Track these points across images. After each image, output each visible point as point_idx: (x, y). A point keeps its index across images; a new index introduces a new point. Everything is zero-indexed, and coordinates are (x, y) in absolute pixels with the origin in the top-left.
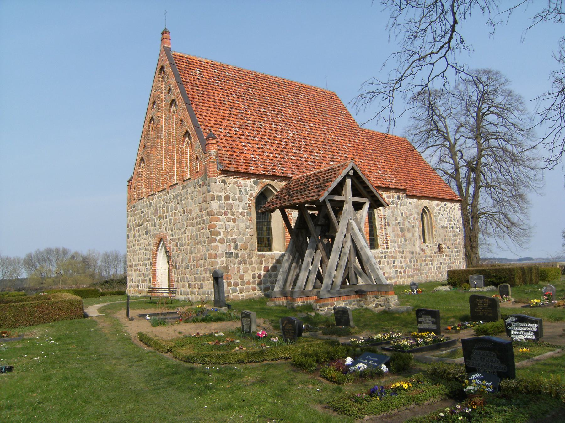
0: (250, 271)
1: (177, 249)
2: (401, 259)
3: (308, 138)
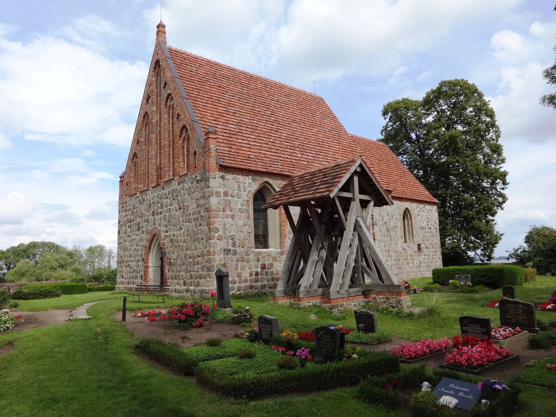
0: (247, 269)
1: (171, 246)
2: (387, 258)
3: (300, 138)
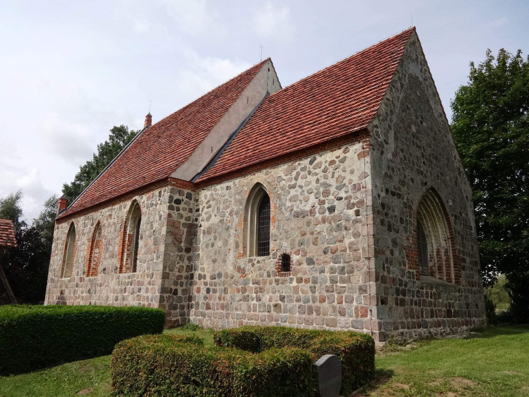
2: (148, 286)
